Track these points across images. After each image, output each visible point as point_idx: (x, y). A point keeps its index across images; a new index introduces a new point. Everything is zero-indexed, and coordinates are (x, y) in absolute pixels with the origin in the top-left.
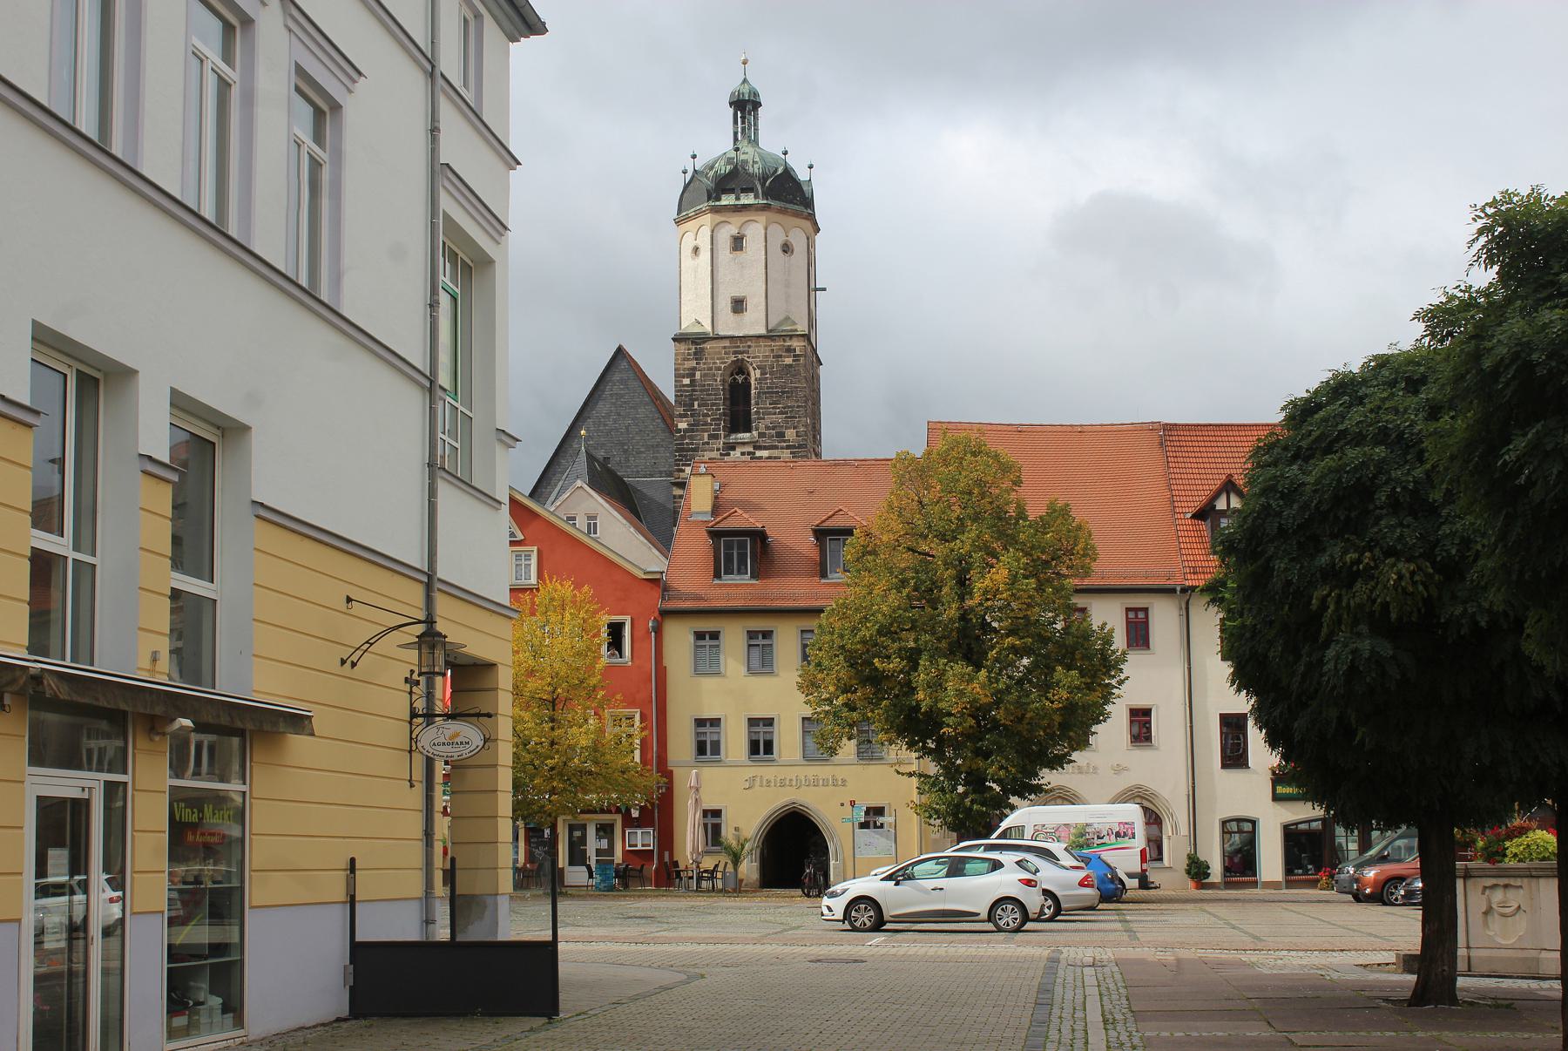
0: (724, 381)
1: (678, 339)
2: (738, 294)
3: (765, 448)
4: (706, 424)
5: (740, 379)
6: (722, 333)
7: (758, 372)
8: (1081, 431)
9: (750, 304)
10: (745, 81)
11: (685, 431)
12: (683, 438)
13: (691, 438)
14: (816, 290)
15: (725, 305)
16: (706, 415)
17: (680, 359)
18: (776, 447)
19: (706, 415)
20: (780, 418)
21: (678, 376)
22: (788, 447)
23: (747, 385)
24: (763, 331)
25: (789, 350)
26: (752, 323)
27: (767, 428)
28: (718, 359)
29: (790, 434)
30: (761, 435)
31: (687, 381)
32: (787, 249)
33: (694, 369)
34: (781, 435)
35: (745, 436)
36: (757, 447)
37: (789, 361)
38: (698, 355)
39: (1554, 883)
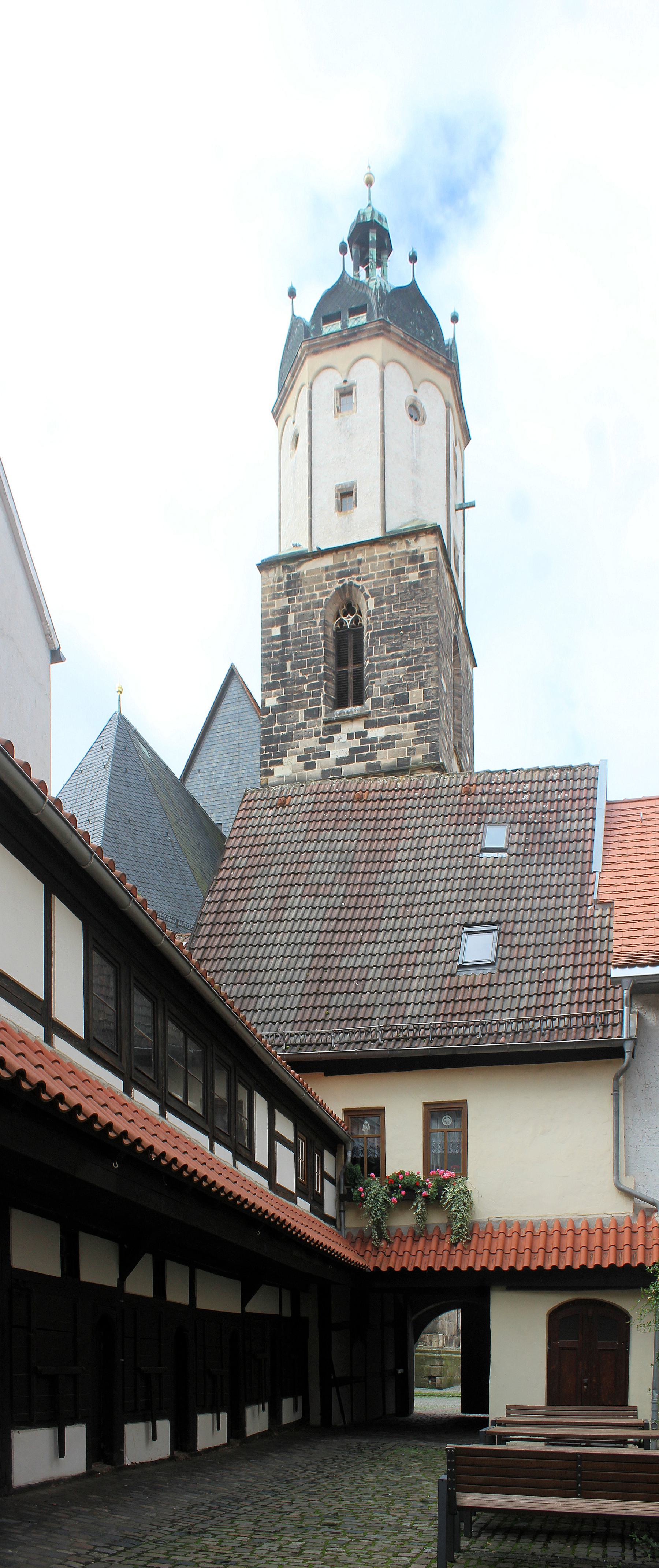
0: (325, 623)
1: (264, 566)
2: (344, 480)
3: (382, 723)
4: (301, 695)
5: (348, 620)
6: (323, 547)
7: (371, 601)
8: (628, 1348)
9: (361, 495)
10: (369, 205)
11: (275, 709)
12: (271, 721)
13: (282, 720)
14: (462, 507)
15: (326, 498)
16: (302, 681)
17: (270, 595)
18: (394, 721)
19: (302, 681)
20: (400, 672)
21: (266, 624)
22: (412, 718)
23: (357, 630)
24: (377, 534)
25: (415, 558)
26: (363, 524)
27: (384, 690)
28: (319, 581)
29: (415, 696)
30: (376, 703)
31: (276, 631)
32: (415, 412)
33: (286, 610)
34: (402, 700)
35: (355, 710)
36: (369, 725)
37: (413, 576)
38: (292, 586)
39: (240, 1312)
